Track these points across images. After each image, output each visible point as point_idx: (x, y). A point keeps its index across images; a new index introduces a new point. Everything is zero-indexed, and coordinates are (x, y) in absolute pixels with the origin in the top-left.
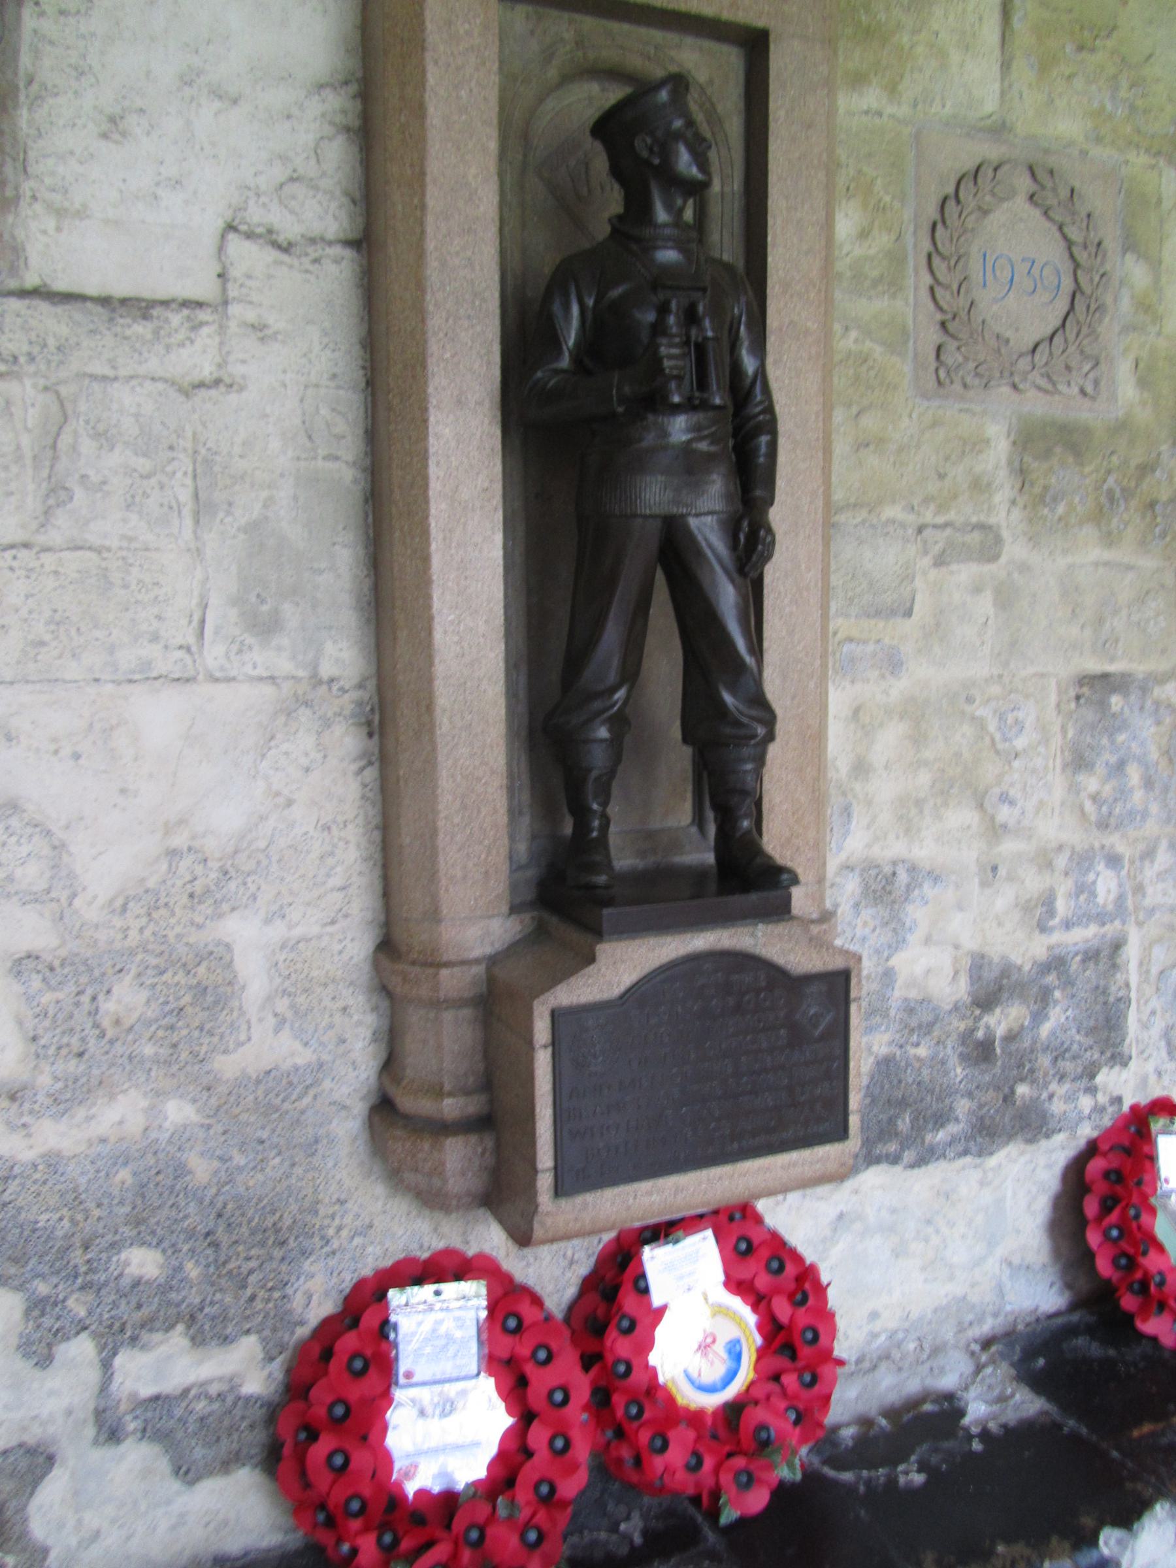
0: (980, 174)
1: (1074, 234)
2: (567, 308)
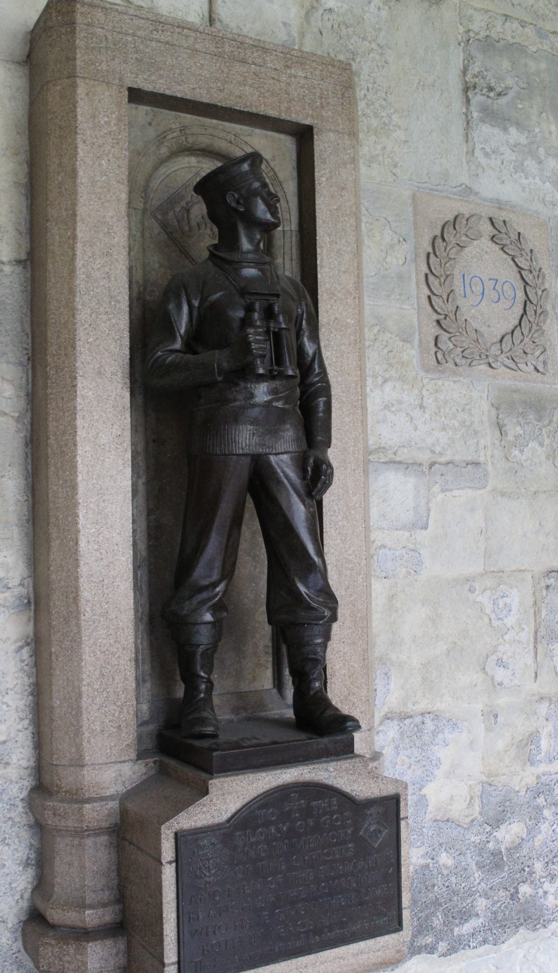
0: (457, 222)
1: (523, 264)
2: (179, 307)
